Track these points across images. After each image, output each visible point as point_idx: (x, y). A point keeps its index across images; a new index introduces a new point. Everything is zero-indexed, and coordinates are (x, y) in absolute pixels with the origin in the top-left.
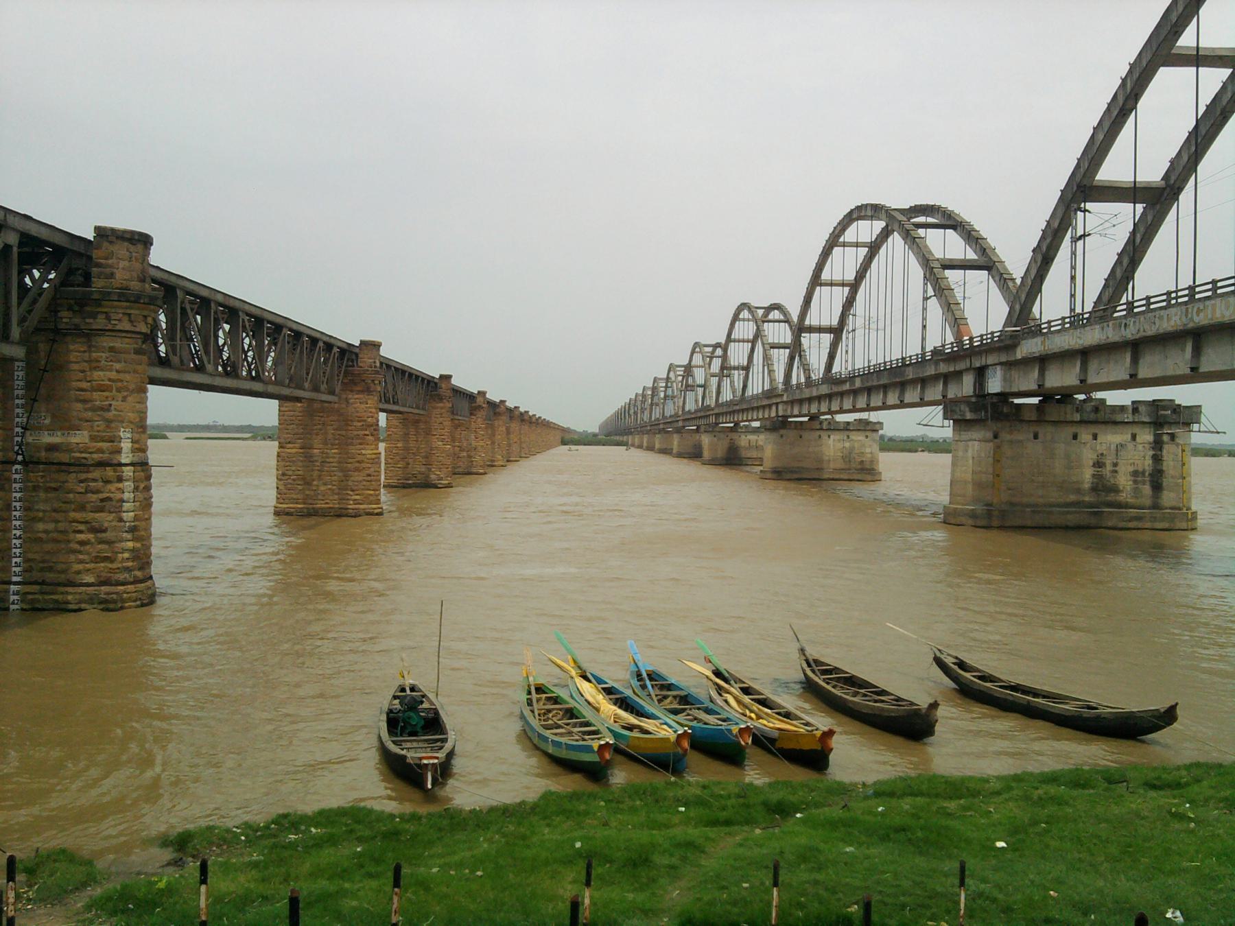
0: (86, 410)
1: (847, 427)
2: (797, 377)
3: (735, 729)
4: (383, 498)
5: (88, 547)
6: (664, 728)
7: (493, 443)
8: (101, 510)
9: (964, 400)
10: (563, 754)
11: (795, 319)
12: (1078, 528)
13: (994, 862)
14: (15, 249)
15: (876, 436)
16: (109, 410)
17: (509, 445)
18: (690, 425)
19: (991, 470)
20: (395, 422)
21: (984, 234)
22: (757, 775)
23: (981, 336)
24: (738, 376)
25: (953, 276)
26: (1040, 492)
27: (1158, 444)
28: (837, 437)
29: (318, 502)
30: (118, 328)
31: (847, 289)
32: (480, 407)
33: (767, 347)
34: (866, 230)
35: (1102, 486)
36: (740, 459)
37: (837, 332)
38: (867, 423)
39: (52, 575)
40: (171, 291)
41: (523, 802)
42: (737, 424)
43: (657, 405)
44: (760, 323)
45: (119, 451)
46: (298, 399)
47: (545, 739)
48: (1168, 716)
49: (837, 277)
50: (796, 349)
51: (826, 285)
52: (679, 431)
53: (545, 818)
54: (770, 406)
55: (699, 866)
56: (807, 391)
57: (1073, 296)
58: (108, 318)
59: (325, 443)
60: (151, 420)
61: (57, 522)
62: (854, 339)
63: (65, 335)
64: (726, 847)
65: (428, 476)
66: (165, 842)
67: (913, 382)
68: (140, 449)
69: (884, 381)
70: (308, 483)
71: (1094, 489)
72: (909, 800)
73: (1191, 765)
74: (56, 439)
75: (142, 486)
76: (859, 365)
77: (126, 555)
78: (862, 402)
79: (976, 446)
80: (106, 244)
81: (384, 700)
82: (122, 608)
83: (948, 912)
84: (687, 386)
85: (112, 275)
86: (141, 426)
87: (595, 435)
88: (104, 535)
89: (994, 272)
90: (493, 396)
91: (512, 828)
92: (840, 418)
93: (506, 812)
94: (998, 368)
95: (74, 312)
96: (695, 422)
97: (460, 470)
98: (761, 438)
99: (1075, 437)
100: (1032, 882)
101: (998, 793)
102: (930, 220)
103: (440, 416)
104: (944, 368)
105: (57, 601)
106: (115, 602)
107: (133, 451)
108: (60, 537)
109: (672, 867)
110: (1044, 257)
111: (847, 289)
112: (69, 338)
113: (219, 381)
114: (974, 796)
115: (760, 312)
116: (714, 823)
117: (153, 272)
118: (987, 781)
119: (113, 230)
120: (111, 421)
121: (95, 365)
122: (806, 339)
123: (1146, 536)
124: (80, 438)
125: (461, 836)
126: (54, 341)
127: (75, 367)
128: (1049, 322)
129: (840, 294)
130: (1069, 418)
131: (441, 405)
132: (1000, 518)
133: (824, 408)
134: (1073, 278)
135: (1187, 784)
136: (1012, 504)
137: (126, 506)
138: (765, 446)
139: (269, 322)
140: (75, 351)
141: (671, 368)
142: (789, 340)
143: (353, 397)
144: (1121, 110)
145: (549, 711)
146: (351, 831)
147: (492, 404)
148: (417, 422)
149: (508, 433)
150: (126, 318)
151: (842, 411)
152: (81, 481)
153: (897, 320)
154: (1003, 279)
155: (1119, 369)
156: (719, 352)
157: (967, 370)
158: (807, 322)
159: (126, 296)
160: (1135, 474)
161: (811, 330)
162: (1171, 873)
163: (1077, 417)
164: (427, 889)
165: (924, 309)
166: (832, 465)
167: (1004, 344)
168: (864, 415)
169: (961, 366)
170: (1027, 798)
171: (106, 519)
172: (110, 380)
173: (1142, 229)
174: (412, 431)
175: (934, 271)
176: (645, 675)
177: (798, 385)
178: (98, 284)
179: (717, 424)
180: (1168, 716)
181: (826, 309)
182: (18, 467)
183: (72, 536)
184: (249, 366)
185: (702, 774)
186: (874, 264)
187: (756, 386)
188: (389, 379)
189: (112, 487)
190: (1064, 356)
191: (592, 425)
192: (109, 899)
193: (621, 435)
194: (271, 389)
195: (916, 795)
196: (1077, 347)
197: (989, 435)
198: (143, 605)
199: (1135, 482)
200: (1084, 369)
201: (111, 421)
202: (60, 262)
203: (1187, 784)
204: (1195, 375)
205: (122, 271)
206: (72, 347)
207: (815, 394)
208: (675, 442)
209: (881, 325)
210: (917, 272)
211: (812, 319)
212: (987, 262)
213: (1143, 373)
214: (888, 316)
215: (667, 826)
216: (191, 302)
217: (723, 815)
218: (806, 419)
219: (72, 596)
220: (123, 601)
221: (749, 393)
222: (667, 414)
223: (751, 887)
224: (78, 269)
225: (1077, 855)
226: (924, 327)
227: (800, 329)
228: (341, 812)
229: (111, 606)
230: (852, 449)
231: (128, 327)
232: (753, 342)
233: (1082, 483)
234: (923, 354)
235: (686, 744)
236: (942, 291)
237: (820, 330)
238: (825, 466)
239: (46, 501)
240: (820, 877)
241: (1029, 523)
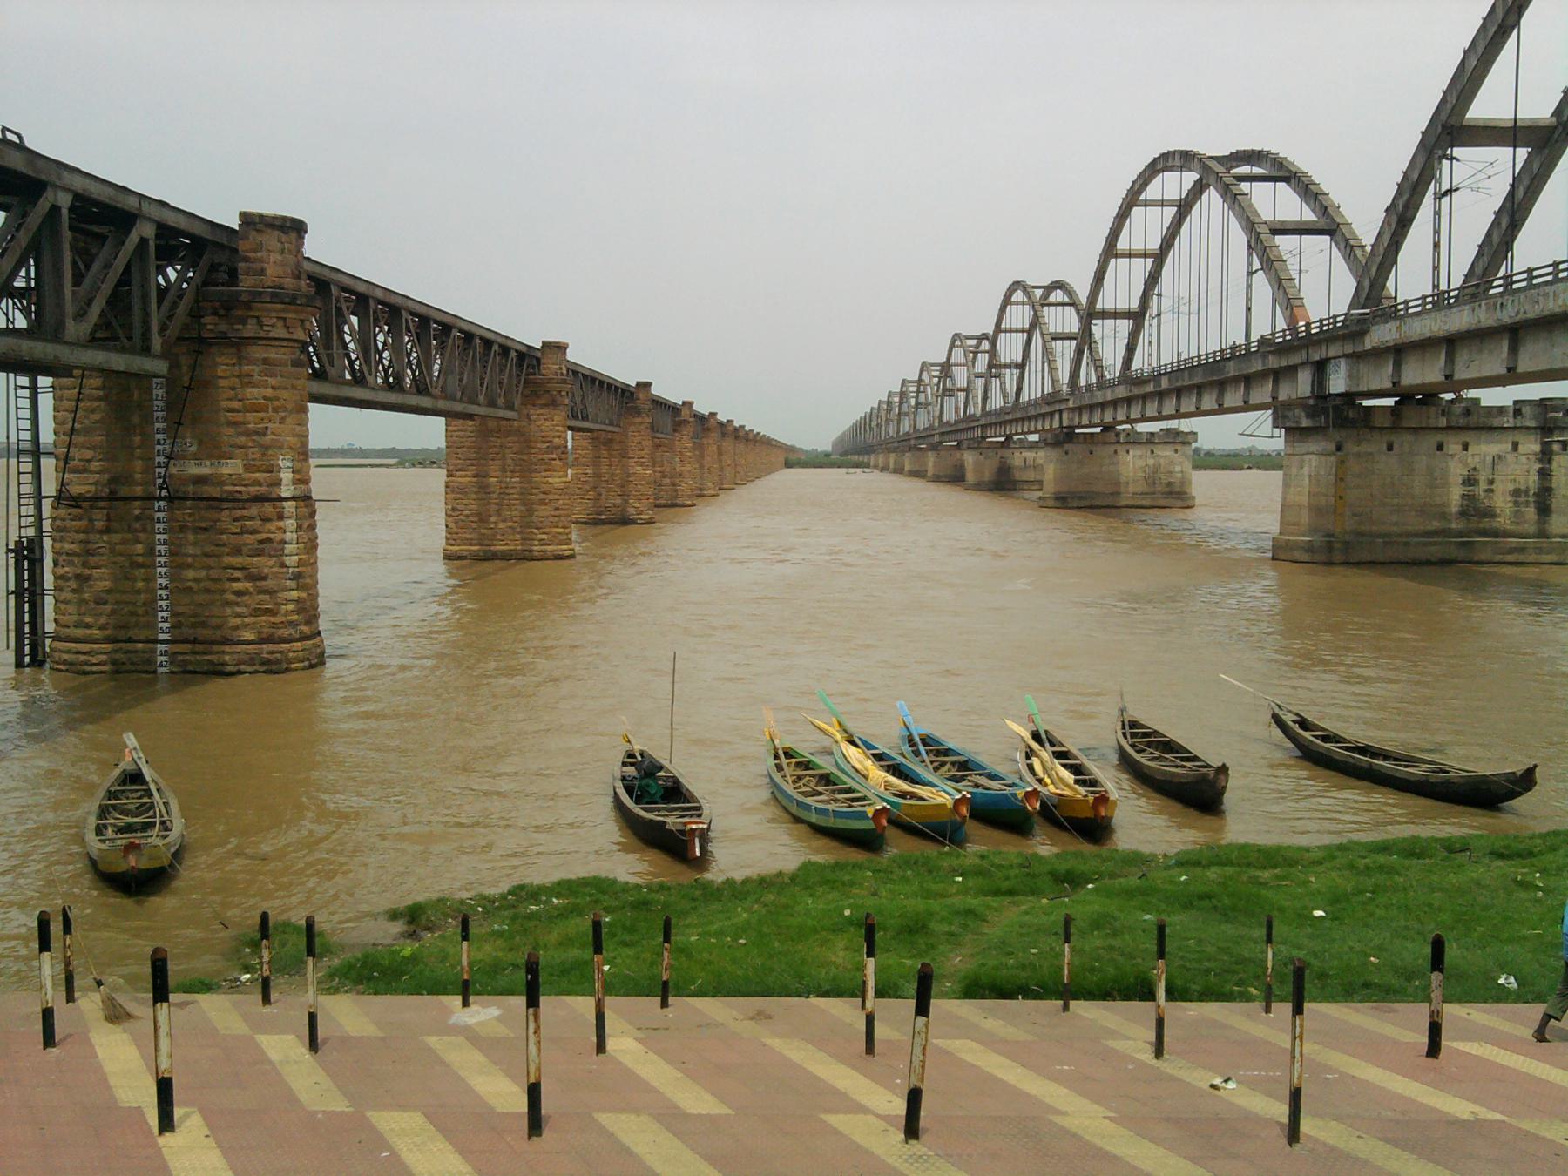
0: (239, 434)
2: (1087, 376)
3: (1020, 793)
4: (574, 536)
6: (941, 794)
7: (702, 466)
9: (1301, 403)
10: (831, 822)
11: (1084, 301)
12: (1445, 562)
13: (1309, 930)
14: (152, 243)
15: (1189, 450)
16: (265, 435)
17: (721, 469)
18: (953, 441)
20: (584, 443)
21: (1325, 188)
22: (1045, 846)
23: (1321, 321)
24: (1010, 377)
25: (1285, 243)
26: (1395, 518)
27: (1546, 455)
28: (1139, 453)
29: (494, 547)
30: (272, 335)
31: (1150, 261)
32: (685, 421)
33: (1048, 338)
34: (1175, 184)
35: (1474, 509)
36: (1015, 482)
37: (1137, 317)
38: (1176, 433)
39: (205, 632)
40: (331, 294)
41: (780, 873)
42: (1009, 438)
43: (907, 414)
44: (1038, 307)
46: (470, 416)
47: (807, 807)
48: (1526, 781)
49: (1138, 246)
50: (1084, 340)
51: (1123, 256)
52: (934, 447)
53: (806, 888)
54: (1052, 414)
55: (982, 934)
56: (1099, 393)
57: (1436, 268)
58: (260, 324)
59: (504, 470)
60: (314, 443)
61: (209, 568)
62: (1159, 326)
63: (211, 344)
64: (1007, 917)
65: (624, 510)
66: (394, 915)
67: (1236, 380)
68: (302, 479)
70: (483, 519)
71: (1463, 513)
72: (1214, 869)
73: (1548, 834)
74: (205, 470)
75: (306, 524)
76: (1166, 359)
77: (291, 607)
78: (1169, 407)
79: (1314, 461)
81: (610, 771)
82: (288, 670)
83: (1257, 977)
85: (262, 272)
86: (303, 453)
87: (827, 455)
89: (1338, 237)
90: (702, 408)
91: (772, 897)
92: (1142, 428)
93: (764, 883)
95: (220, 317)
97: (662, 502)
98: (1041, 456)
99: (1440, 447)
100: (1351, 948)
101: (1320, 863)
102: (1257, 170)
103: (637, 435)
104: (1273, 362)
105: (211, 662)
106: (278, 662)
107: (296, 482)
108: (213, 586)
109: (952, 935)
110: (1400, 218)
111: (1150, 261)
112: (214, 349)
114: (1291, 866)
115: (1039, 293)
116: (997, 893)
117: (307, 266)
118: (1308, 850)
119: (261, 216)
120: (267, 448)
121: (246, 380)
122: (1097, 327)
123: (1530, 572)
124: (232, 468)
125: (717, 906)
126: (198, 352)
127: (223, 383)
128: (1406, 302)
129: (1142, 267)
130: (1432, 423)
131: (638, 420)
132: (1340, 550)
133: (1121, 416)
134: (1436, 246)
135: (1541, 853)
136: (1362, 534)
137: (289, 548)
138: (1048, 467)
139: (436, 322)
140: (223, 366)
141: (924, 367)
142: (1075, 329)
143: (535, 413)
144: (1500, 26)
145: (800, 778)
146: (597, 902)
147: (701, 419)
148: (611, 441)
149: (720, 453)
150: (280, 324)
151: (1144, 419)
152: (236, 520)
153: (1213, 302)
155: (1494, 360)
156: (985, 345)
158: (1099, 306)
159: (281, 297)
160: (1516, 493)
161: (1104, 315)
162: (1510, 941)
163: (1443, 422)
164: (689, 956)
165: (1249, 286)
166: (1131, 489)
167: (1348, 331)
168: (1173, 424)
169: (1295, 359)
170: (1352, 867)
171: (265, 564)
172: (265, 398)
173: (1526, 182)
174: (605, 454)
175: (1262, 239)
176: (917, 739)
177: (1088, 386)
178: (246, 282)
179: (984, 438)
180: (1526, 781)
181: (1123, 286)
182: (162, 503)
183: (227, 585)
184: (386, 371)
185: (982, 844)
186: (1185, 229)
187: (1034, 389)
188: (578, 392)
189: (272, 526)
190: (1424, 346)
191: (822, 439)
192: (351, 967)
193: (859, 453)
194: (442, 404)
195: (1225, 865)
196: (1441, 334)
197: (1332, 447)
198: (312, 666)
199: (1516, 503)
200: (1450, 359)
201: (267, 448)
202: (200, 257)
203: (1541, 853)
204: (1199, 413)
205: (274, 266)
206: (218, 360)
208: (931, 460)
210: (1239, 239)
211: (1105, 302)
212: (1329, 225)
213: (1524, 366)
214: (1203, 295)
215: (942, 895)
216: (347, 300)
217: (1005, 885)
218: (1098, 430)
219: (229, 656)
220: (290, 661)
221: (1024, 398)
222: (921, 426)
223: (1040, 953)
224: (220, 265)
225: (1403, 923)
226: (1249, 309)
227: (1090, 314)
228: (584, 883)
229: (274, 667)
230: (1156, 468)
231: (282, 333)
232: (1029, 332)
233: (1449, 506)
234: (1248, 345)
235: (964, 810)
236: (1270, 263)
237: (1115, 315)
238: (1122, 489)
239: (195, 544)
240: (1115, 942)
241: (1381, 558)
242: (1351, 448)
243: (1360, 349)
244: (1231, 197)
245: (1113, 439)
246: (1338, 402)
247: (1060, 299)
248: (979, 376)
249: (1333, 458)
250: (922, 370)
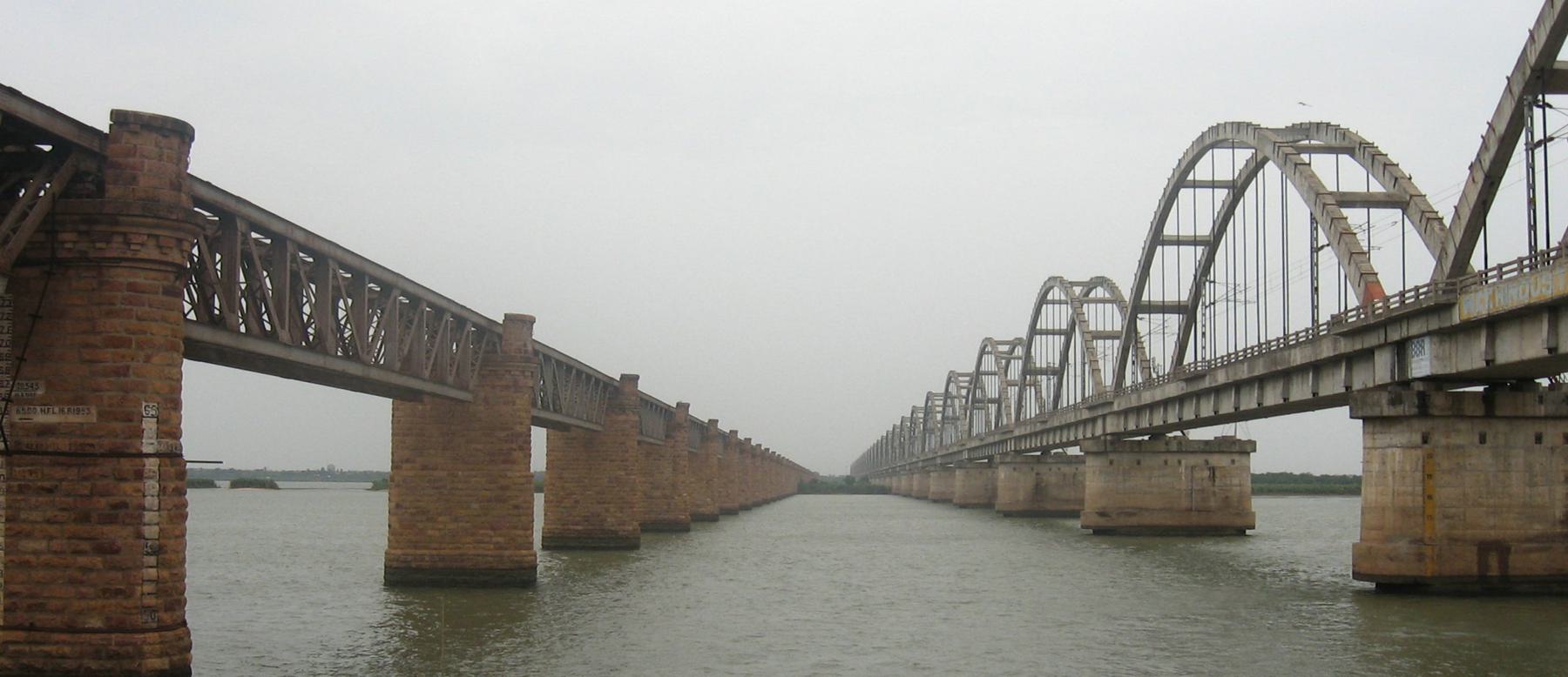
1: (1208, 447)
5: (93, 575)
8: (110, 520)
11: (1127, 295)
19: (1419, 489)
25: (1355, 216)
26: (1492, 521)
30: (141, 255)
33: (1088, 337)
37: (1187, 312)
39: (42, 616)
40: (229, 219)
45: (139, 434)
50: (1130, 339)
54: (1093, 420)
58: (128, 243)
61: (51, 538)
69: (1260, 370)
77: (148, 588)
80: (126, 136)
84: (975, 400)
88: (117, 557)
92: (1196, 434)
94: (1427, 340)
104: (1345, 347)
105: (48, 655)
113: (297, 356)
115: (1078, 290)
119: (136, 115)
128: (1500, 267)
129: (1190, 257)
130: (1530, 411)
134: (1532, 202)
137: (149, 516)
141: (952, 378)
142: (1118, 327)
150: (152, 243)
152: (85, 479)
153: (1276, 286)
154: (1427, 220)
157: (1380, 347)
158: (1145, 298)
161: (1152, 308)
165: (1314, 265)
171: (118, 534)
172: (127, 330)
175: (1330, 208)
181: (1172, 276)
189: (127, 487)
191: (835, 462)
197: (1417, 438)
207: (1158, 398)
209: (1252, 295)
210: (1300, 211)
211: (1153, 293)
212: (1401, 197)
231: (155, 254)
232: (1068, 334)
237: (1164, 308)
242: (1439, 439)
243: (1447, 324)
244: (1297, 170)
245: (1163, 448)
246: (1419, 387)
249: (1419, 452)
250: (949, 381)
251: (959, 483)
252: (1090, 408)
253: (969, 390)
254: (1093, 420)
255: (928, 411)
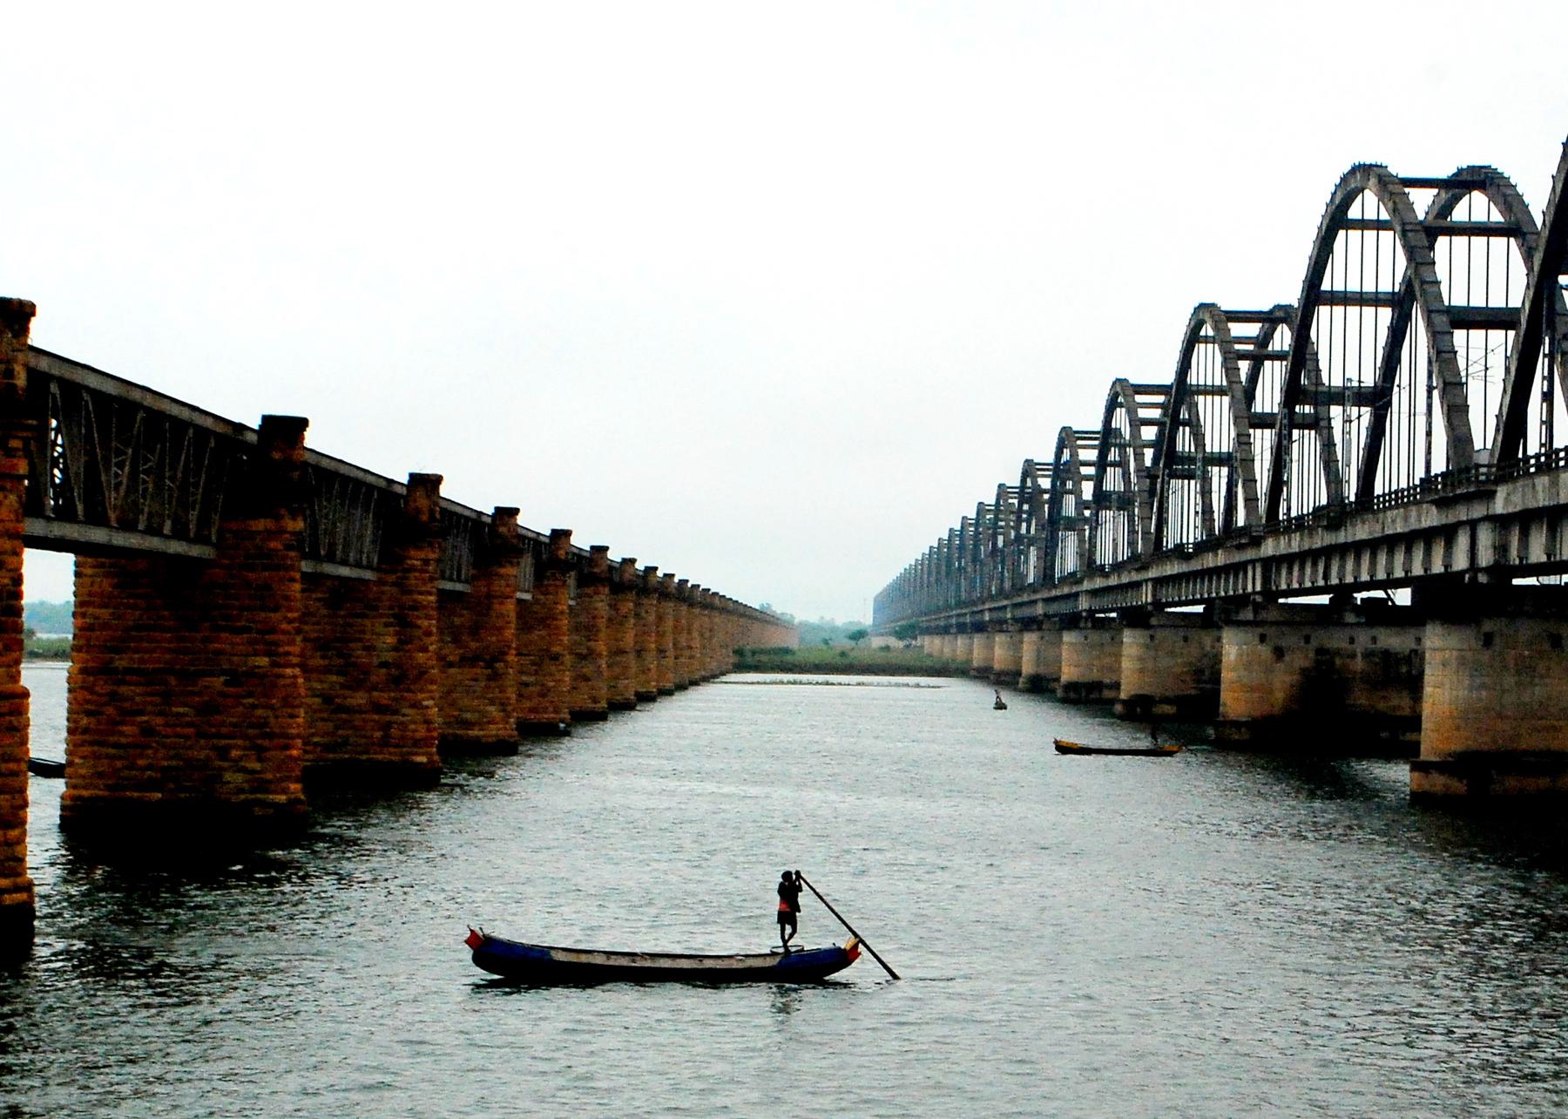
33: (1441, 321)
43: (1071, 524)
52: (1136, 618)
54: (1447, 533)
96: (1203, 589)
141: (1122, 394)
222: (1105, 556)
247: (1479, 216)
248: (1264, 421)
251: (1133, 662)
252: (1443, 504)
253: (1152, 437)
254: (1447, 533)
255: (1063, 471)
